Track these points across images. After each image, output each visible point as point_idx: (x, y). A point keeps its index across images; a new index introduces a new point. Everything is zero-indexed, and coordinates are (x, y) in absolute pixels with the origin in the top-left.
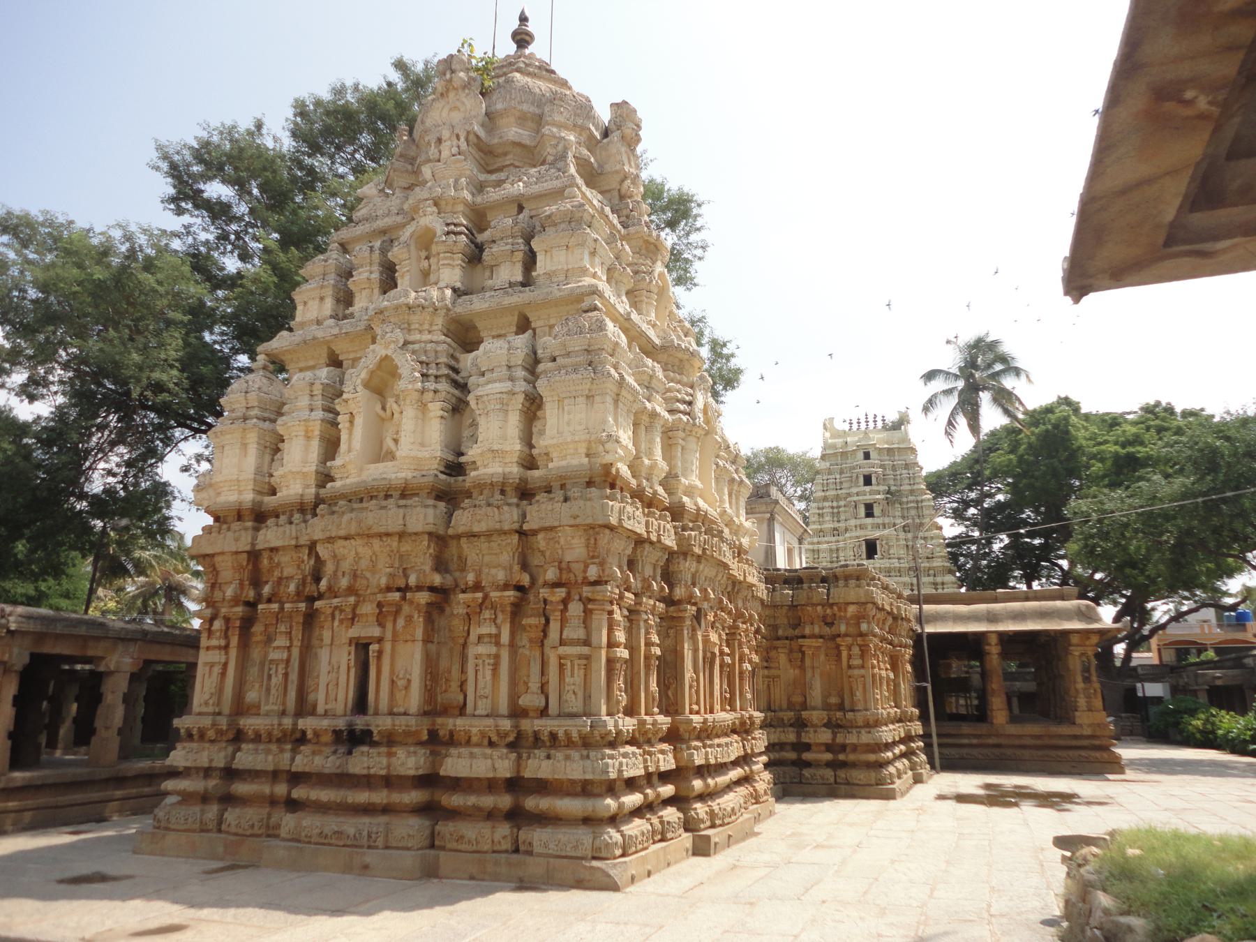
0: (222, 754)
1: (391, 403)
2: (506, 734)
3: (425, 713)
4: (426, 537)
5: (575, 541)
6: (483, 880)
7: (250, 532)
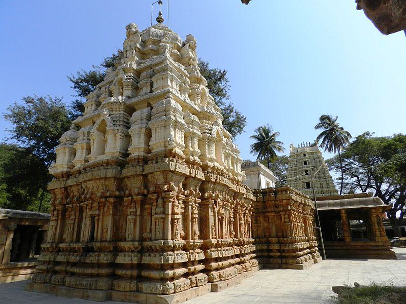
2: (137, 248)
5: (160, 177)
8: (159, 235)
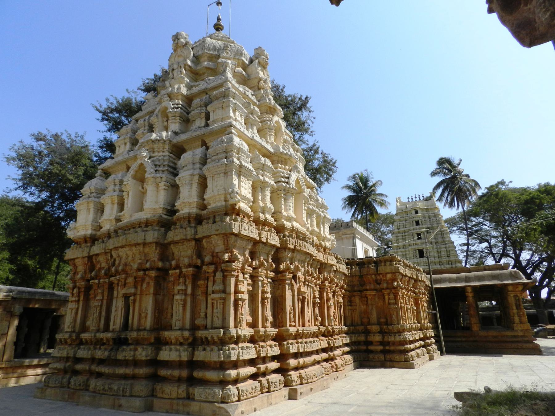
2: (188, 339)
4: (155, 244)
5: (219, 242)
6: (171, 413)
8: (218, 322)
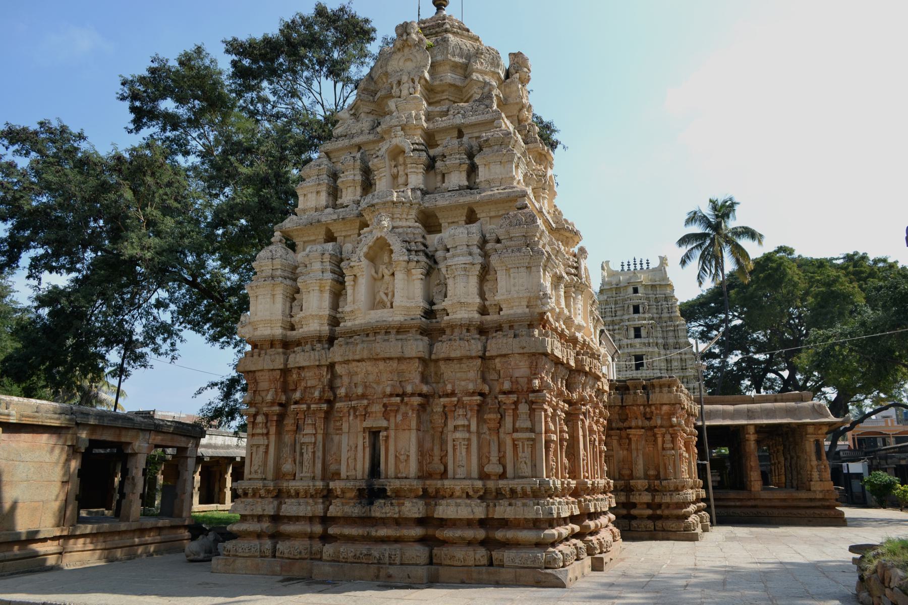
0: (271, 506)
1: (383, 269)
3: (419, 478)
7: (282, 356)
8: (526, 470)
